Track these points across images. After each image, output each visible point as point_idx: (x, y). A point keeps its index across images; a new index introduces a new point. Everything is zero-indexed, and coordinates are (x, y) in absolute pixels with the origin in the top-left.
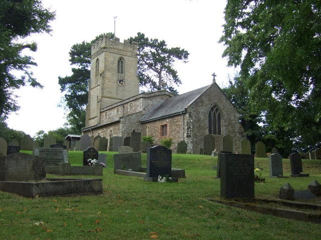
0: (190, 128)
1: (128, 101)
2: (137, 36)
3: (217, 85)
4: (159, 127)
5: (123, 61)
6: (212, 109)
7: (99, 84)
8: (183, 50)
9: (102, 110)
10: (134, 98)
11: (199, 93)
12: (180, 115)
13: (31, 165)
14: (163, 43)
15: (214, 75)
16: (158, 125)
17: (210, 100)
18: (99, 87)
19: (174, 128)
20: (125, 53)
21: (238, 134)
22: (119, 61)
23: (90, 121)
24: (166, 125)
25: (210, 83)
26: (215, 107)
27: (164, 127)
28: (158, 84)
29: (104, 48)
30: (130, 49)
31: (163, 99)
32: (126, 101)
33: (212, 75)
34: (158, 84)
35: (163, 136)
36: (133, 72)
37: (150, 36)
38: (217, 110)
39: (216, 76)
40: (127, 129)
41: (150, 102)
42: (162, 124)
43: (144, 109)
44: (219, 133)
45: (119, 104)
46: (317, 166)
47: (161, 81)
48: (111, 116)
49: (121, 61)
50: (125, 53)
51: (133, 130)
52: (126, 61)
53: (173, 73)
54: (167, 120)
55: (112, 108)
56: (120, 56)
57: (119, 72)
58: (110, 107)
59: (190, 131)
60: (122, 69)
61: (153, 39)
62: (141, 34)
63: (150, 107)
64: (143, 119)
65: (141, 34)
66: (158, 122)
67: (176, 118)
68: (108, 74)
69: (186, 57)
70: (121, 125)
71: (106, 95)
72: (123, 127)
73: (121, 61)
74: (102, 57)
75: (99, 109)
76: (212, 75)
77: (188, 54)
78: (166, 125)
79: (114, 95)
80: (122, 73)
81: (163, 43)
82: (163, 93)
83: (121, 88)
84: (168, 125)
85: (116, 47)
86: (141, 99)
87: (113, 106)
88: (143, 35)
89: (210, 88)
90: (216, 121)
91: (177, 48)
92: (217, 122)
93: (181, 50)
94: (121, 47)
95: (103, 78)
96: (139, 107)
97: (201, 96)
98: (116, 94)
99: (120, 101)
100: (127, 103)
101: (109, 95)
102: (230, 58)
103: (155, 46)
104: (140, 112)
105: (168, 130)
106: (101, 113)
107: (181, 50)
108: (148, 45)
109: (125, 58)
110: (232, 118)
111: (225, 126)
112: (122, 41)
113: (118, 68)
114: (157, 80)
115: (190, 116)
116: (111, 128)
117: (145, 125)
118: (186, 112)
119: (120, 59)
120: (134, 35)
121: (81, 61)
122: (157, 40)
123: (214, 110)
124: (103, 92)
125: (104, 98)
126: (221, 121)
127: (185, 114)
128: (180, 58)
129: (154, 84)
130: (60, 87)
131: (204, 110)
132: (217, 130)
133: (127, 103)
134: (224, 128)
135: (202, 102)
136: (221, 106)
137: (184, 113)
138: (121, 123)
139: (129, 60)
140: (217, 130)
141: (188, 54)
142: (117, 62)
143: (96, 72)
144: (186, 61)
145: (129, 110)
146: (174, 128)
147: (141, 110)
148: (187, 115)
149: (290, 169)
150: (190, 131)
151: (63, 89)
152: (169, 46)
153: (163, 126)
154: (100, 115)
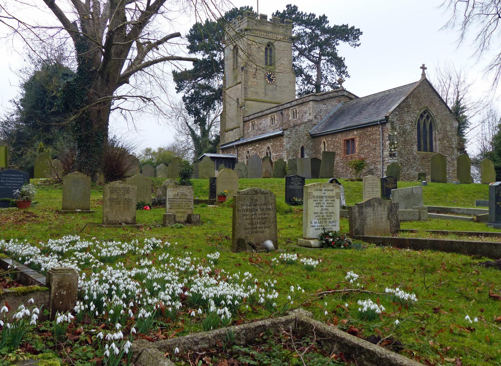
0: (393, 143)
1: (289, 105)
2: (286, 9)
3: (427, 81)
4: (342, 142)
5: (273, 48)
6: (422, 116)
7: (238, 81)
8: (353, 28)
9: (247, 119)
12: (376, 125)
13: (386, 213)
14: (324, 19)
15: (423, 68)
16: (340, 139)
17: (419, 103)
18: (239, 86)
19: (366, 143)
20: (274, 37)
21: (456, 151)
22: (266, 49)
23: (227, 133)
24: (353, 140)
25: (417, 78)
26: (425, 112)
27: (349, 143)
28: (314, 78)
29: (246, 30)
30: (281, 30)
31: (340, 101)
32: (286, 106)
33: (421, 68)
34: (314, 78)
35: (347, 154)
36: (287, 63)
37: (304, 8)
38: (428, 117)
39: (426, 68)
40: (293, 145)
41: (323, 107)
42: (345, 138)
43: (316, 117)
44: (431, 150)
45: (274, 110)
47: (320, 75)
48: (260, 127)
49: (269, 47)
51: (301, 146)
52: (276, 47)
53: (339, 63)
54: (355, 133)
55: (262, 116)
57: (266, 64)
58: (260, 114)
59: (395, 148)
60: (271, 60)
61: (308, 14)
62: (292, 6)
64: (314, 130)
65: (292, 6)
66: (339, 136)
67: (370, 129)
69: (356, 38)
70: (285, 140)
71: (250, 96)
72: (288, 143)
73: (269, 47)
74: (241, 44)
75: (242, 117)
76: (421, 68)
77: (361, 33)
78: (353, 140)
79: (262, 97)
80: (271, 65)
81: (324, 19)
82: (340, 94)
83: (271, 87)
84: (357, 140)
85: (263, 28)
86: (311, 103)
87: (264, 113)
88: (295, 8)
89: (419, 86)
91: (343, 26)
92: (428, 134)
93: (349, 27)
94: (269, 28)
95: (246, 72)
97: (407, 98)
98: (263, 95)
99: (275, 105)
101: (255, 97)
102: (341, 39)
103: (313, 24)
104: (310, 121)
106: (245, 122)
107: (349, 27)
109: (276, 43)
110: (448, 128)
111: (439, 140)
112: (269, 17)
113: (266, 59)
114: (314, 74)
115: (393, 128)
116: (269, 145)
117: (316, 140)
118: (387, 121)
119: (268, 45)
120: (282, 9)
121: (207, 49)
122: (314, 15)
123: (424, 118)
124: (246, 93)
126: (433, 132)
127: (385, 123)
128: (347, 39)
129: (308, 78)
130: (175, 85)
131: (411, 118)
132: (428, 145)
134: (438, 142)
135: (409, 106)
136: (433, 111)
137: (383, 123)
138: (285, 136)
139: (280, 46)
140: (428, 145)
141: (361, 33)
143: (234, 66)
144: (358, 43)
145: (290, 118)
146: (366, 143)
147: (311, 118)
148: (388, 126)
150: (395, 148)
151: (179, 89)
152: (331, 24)
153: (347, 141)
154: (244, 125)
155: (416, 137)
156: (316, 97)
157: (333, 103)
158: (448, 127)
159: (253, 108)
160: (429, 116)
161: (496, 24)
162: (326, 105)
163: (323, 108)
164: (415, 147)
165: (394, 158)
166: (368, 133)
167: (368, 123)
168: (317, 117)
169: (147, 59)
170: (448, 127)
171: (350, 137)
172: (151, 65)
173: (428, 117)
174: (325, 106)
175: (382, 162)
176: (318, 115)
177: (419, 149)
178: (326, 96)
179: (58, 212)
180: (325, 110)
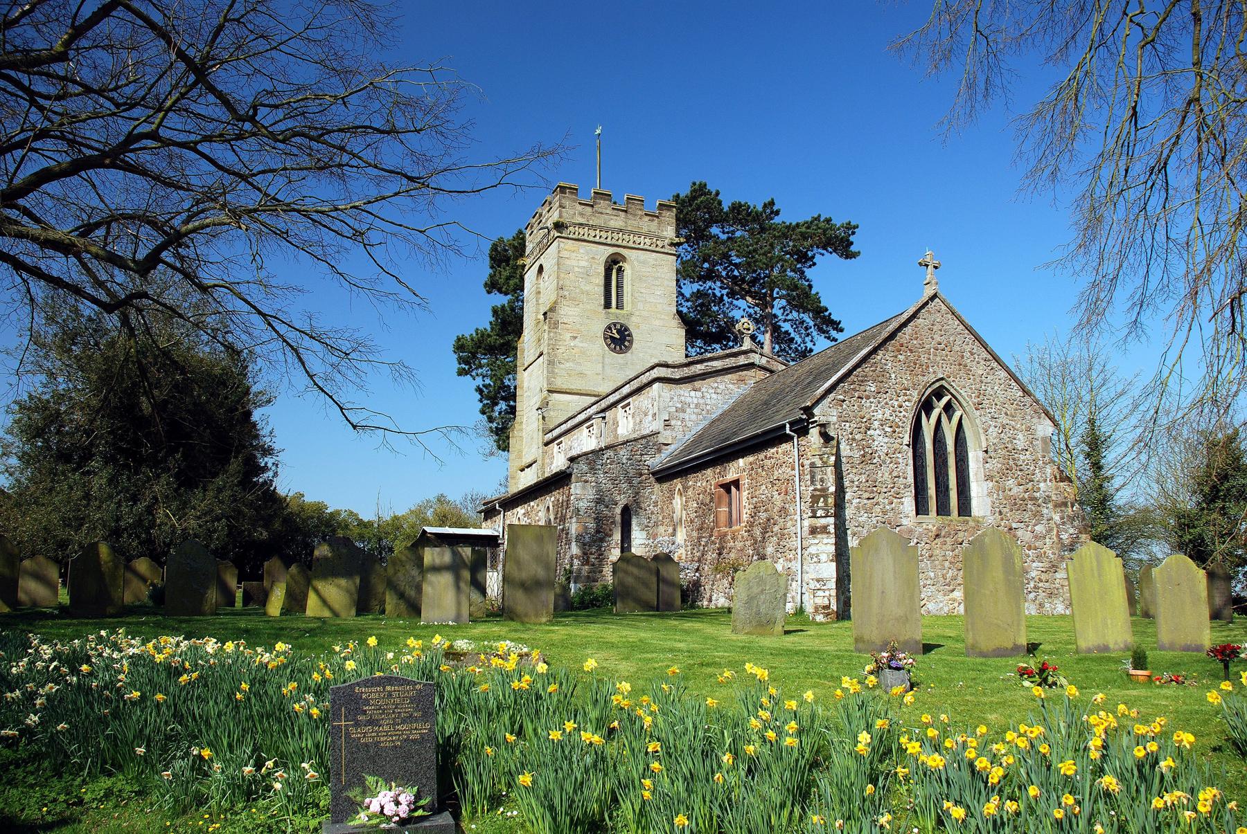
6: (927, 406)
9: (549, 436)
10: (635, 385)
11: (866, 341)
20: (629, 240)
26: (939, 394)
43: (667, 424)
46: (951, 587)
49: (613, 265)
50: (629, 240)
56: (612, 250)
57: (607, 305)
63: (690, 416)
68: (567, 313)
70: (575, 488)
71: (560, 383)
73: (613, 265)
78: (736, 483)
84: (745, 482)
86: (656, 386)
90: (1103, 657)
96: (650, 418)
100: (614, 404)
105: (744, 501)
108: (722, 219)
110: (1021, 442)
120: (685, 192)
125: (555, 395)
133: (614, 404)
142: (602, 270)
149: (699, 475)
155: (910, 470)
156: (670, 370)
157: (722, 387)
158: (1020, 436)
159: (567, 405)
160: (955, 403)
161: (316, 345)
162: (699, 390)
163: (689, 400)
164: (909, 504)
165: (825, 541)
166: (767, 462)
167: (765, 433)
168: (673, 423)
169: (130, 157)
170: (1020, 436)
171: (731, 476)
172: (52, 277)
173: (948, 408)
174: (699, 394)
175: (799, 551)
176: (677, 418)
177: (921, 508)
178: (699, 366)
179: (458, 252)
180: (697, 406)
